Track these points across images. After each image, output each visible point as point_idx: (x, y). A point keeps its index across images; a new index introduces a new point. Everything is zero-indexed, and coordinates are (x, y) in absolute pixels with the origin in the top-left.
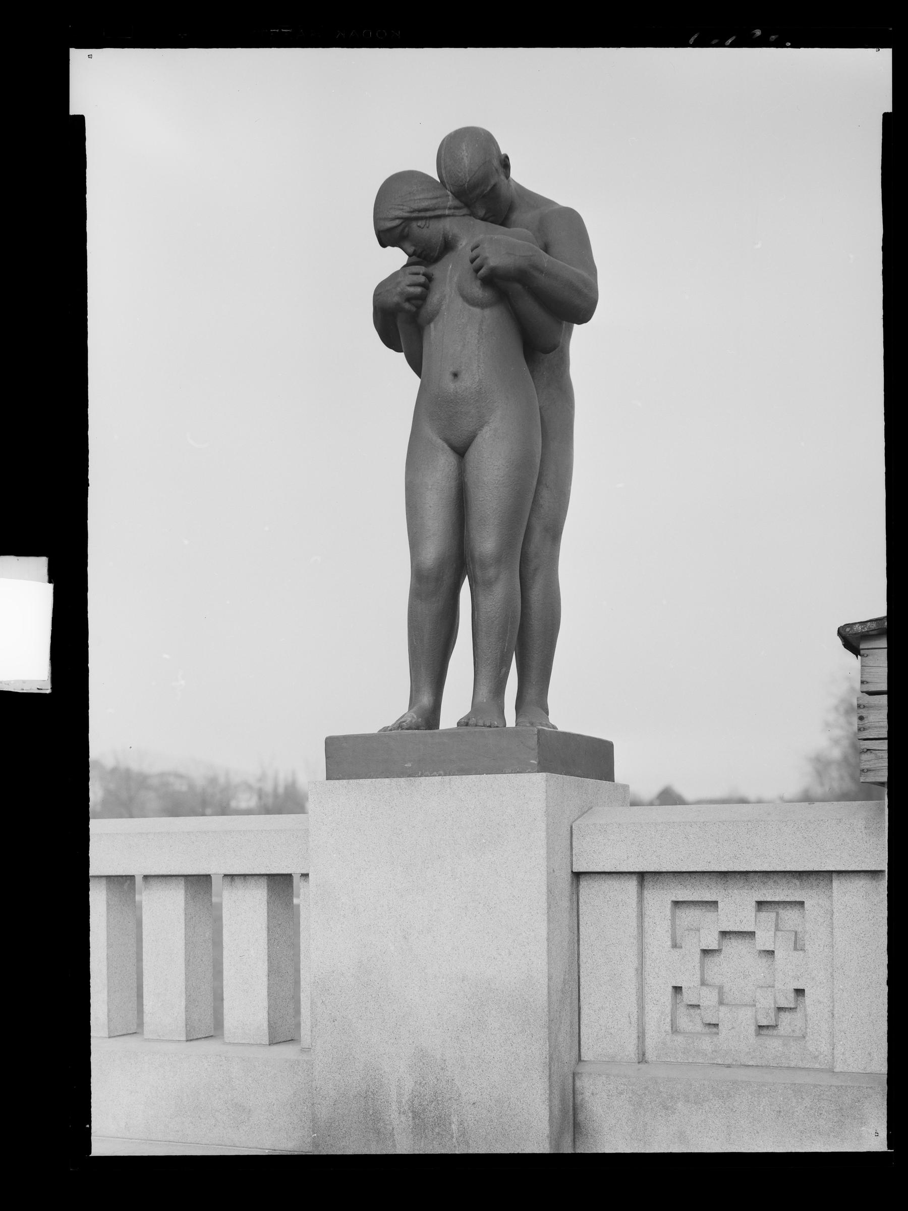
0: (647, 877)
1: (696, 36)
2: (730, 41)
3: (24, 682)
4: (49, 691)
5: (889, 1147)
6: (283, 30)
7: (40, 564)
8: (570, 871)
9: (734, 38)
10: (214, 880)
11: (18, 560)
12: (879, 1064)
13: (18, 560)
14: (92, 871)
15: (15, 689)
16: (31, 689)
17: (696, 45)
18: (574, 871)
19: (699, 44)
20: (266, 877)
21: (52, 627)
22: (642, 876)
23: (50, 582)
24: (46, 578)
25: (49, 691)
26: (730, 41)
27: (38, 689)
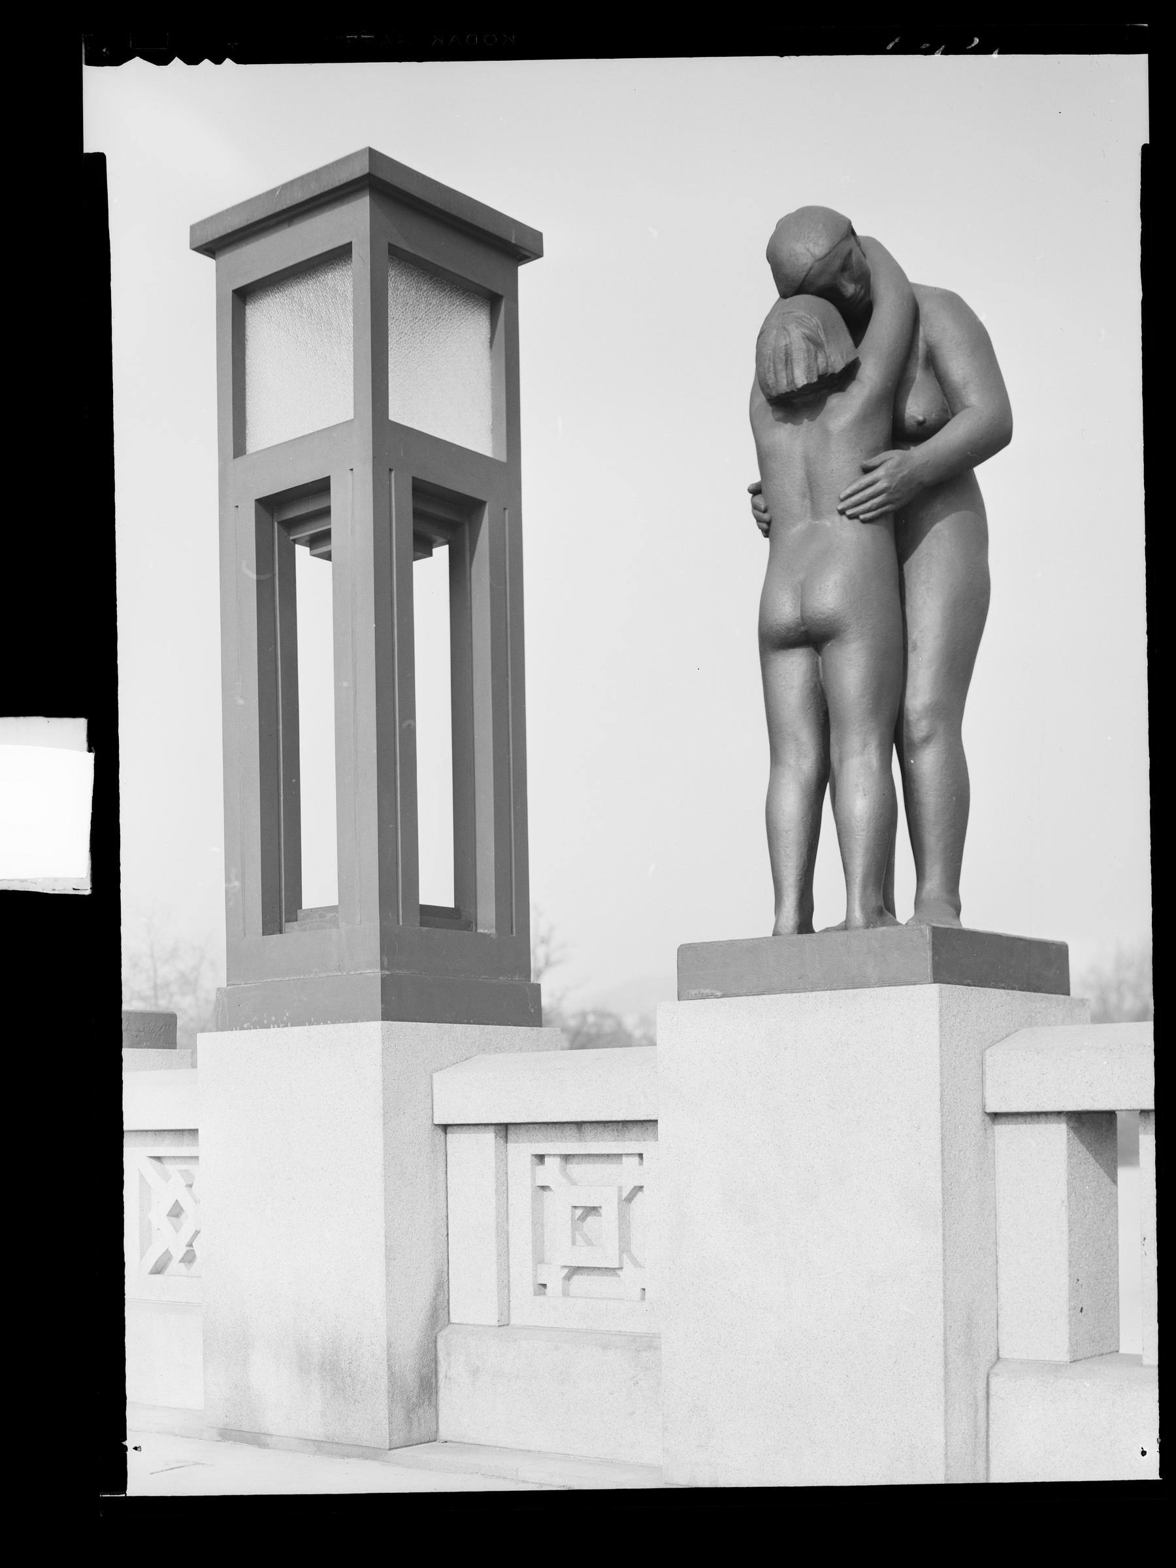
0: (511, 1131)
1: (83, 46)
2: (891, 46)
3: (56, 880)
4: (88, 892)
5: (1160, 1477)
6: (363, 36)
7: (77, 728)
8: (431, 1123)
9: (888, 48)
10: (1120, 1117)
11: (48, 722)
12: (1157, 1363)
13: (48, 722)
14: (125, 1128)
15: (43, 890)
16: (64, 890)
17: (896, 51)
18: (987, 1112)
19: (897, 51)
20: (493, 1127)
21: (93, 809)
22: (504, 1129)
23: (90, 751)
24: (85, 745)
25: (88, 892)
26: (891, 46)
27: (74, 889)
